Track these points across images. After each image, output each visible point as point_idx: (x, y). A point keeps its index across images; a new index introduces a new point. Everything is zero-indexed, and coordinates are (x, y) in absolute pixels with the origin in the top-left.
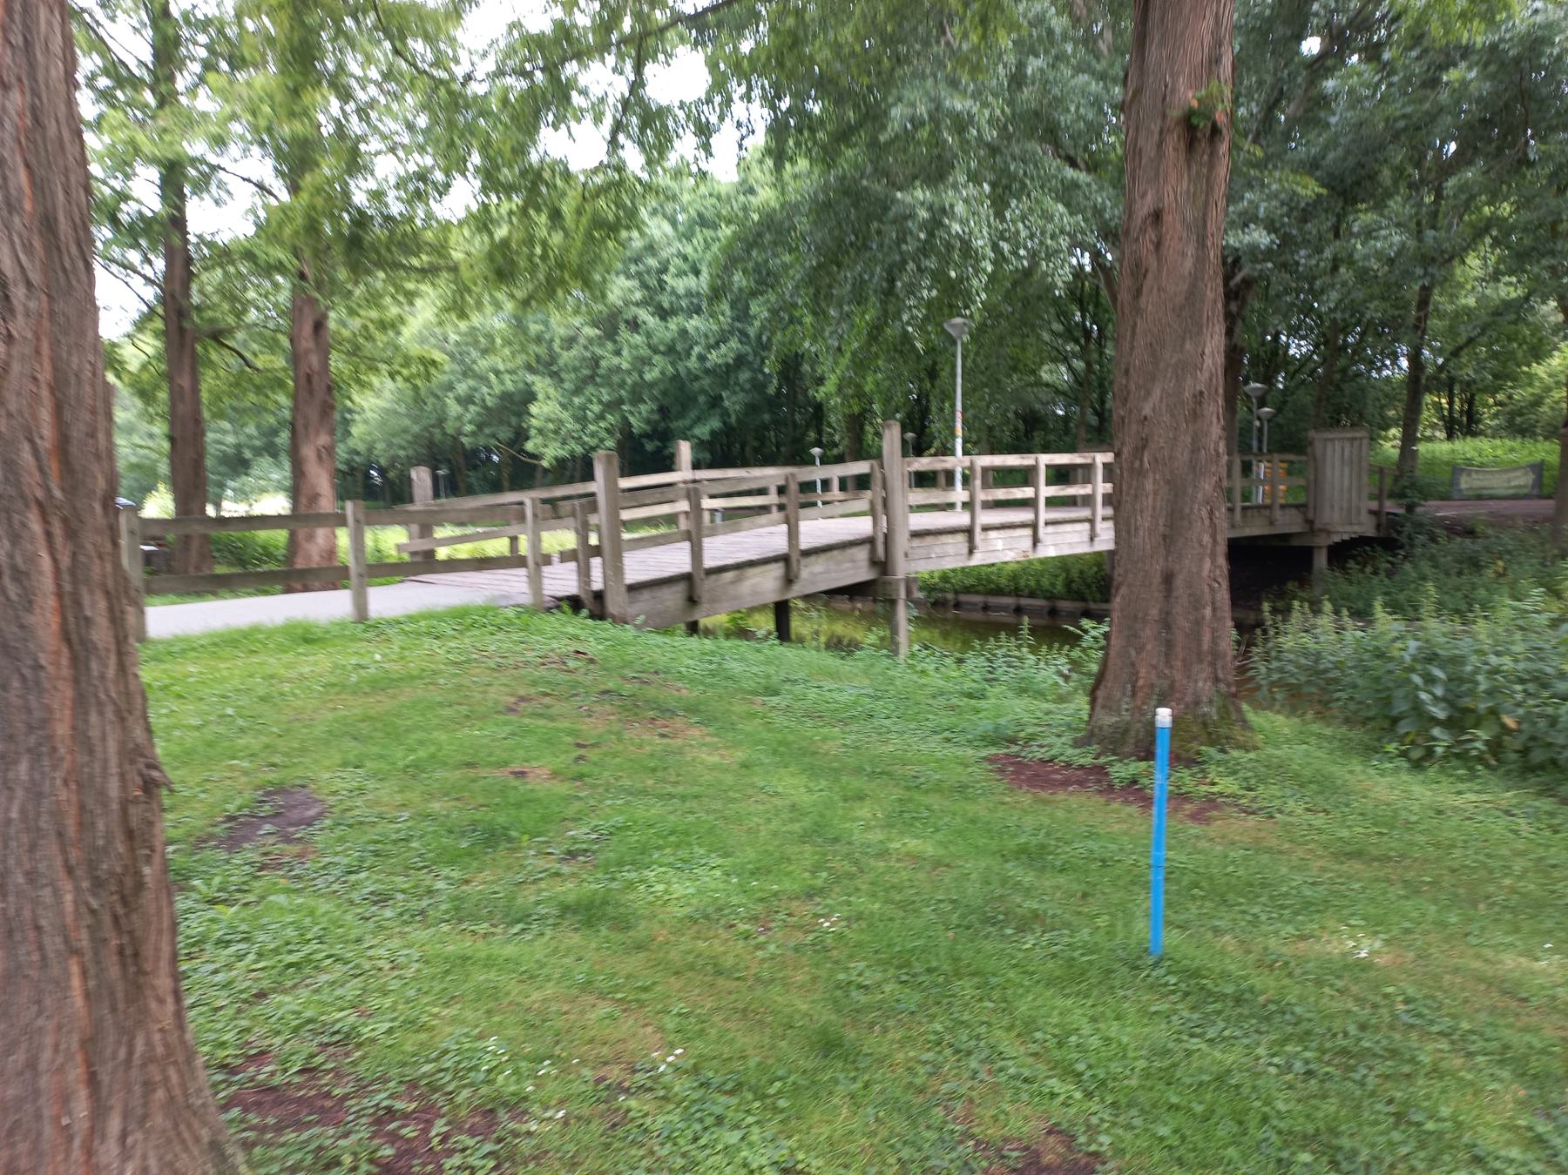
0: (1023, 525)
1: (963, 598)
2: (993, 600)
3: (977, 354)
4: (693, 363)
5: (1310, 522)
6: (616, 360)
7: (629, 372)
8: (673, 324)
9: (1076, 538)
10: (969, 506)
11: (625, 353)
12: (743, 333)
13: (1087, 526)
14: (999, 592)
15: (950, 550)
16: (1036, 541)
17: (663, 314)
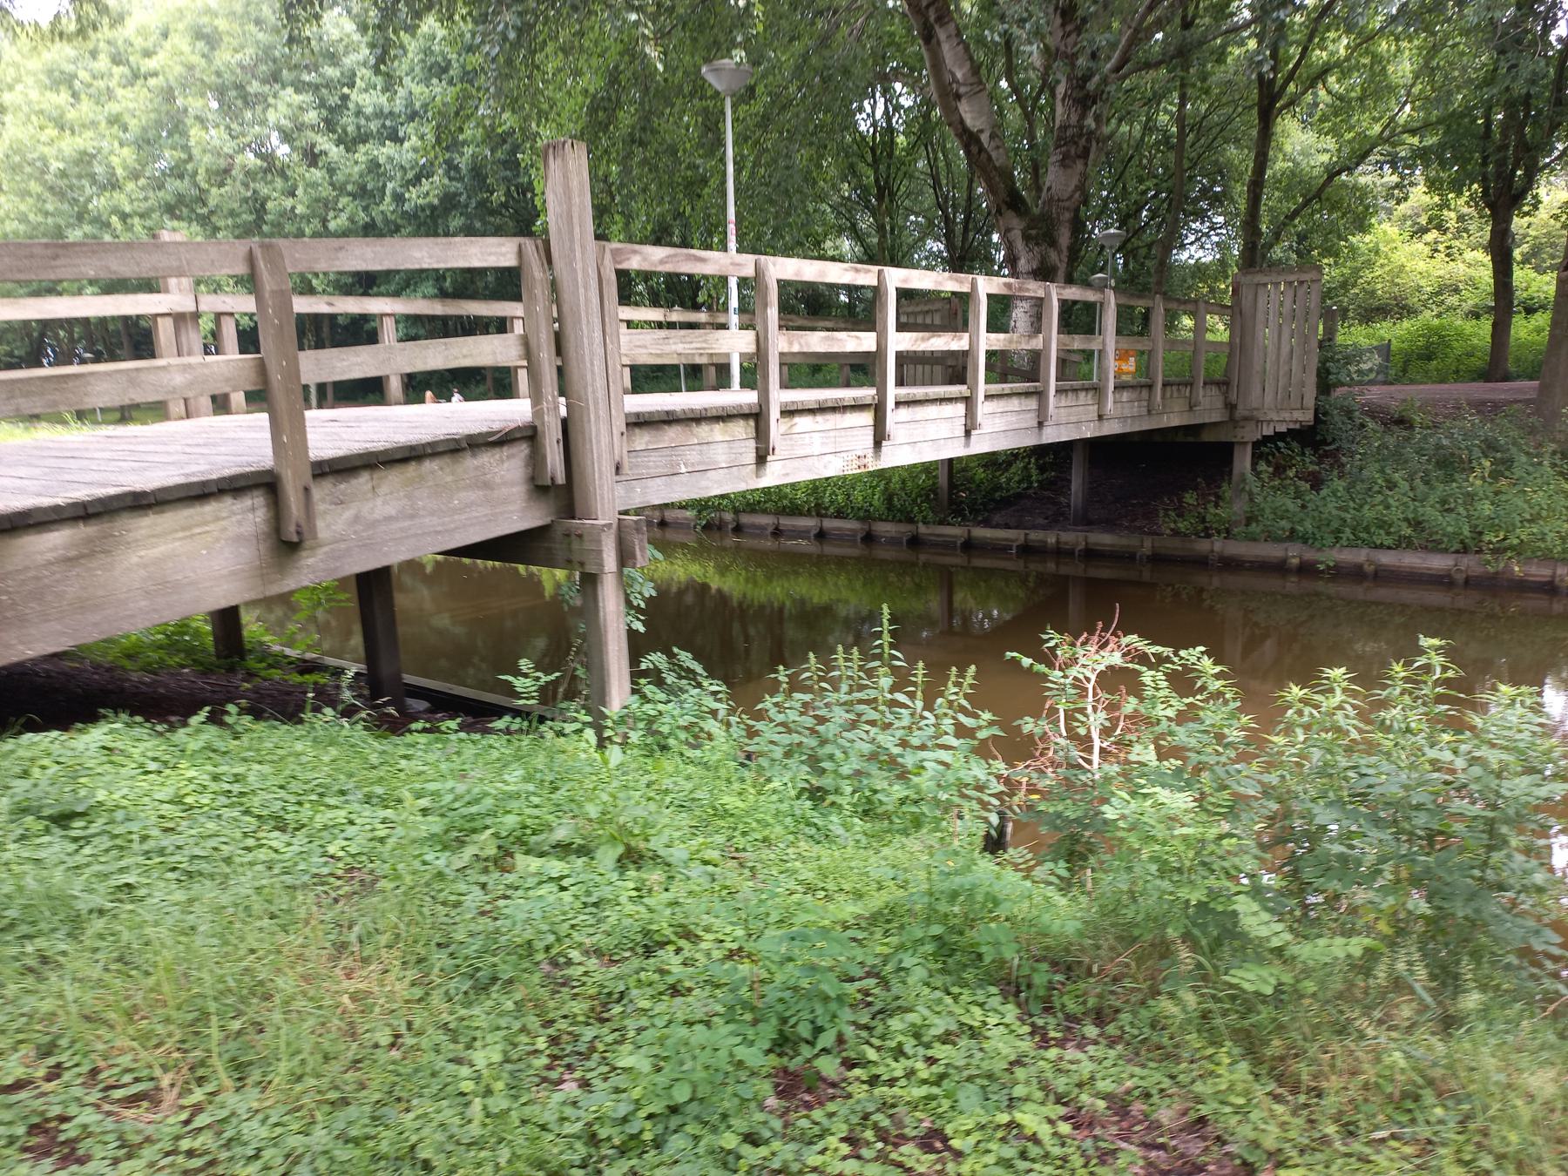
0: (858, 407)
1: (746, 519)
2: (786, 522)
3: (756, 164)
4: (387, 205)
5: (1231, 407)
6: (288, 203)
7: (307, 219)
8: (362, 153)
9: (943, 430)
10: (753, 375)
11: (300, 192)
12: (451, 167)
13: (960, 408)
14: (795, 510)
15: (720, 455)
16: (880, 437)
17: (350, 143)
